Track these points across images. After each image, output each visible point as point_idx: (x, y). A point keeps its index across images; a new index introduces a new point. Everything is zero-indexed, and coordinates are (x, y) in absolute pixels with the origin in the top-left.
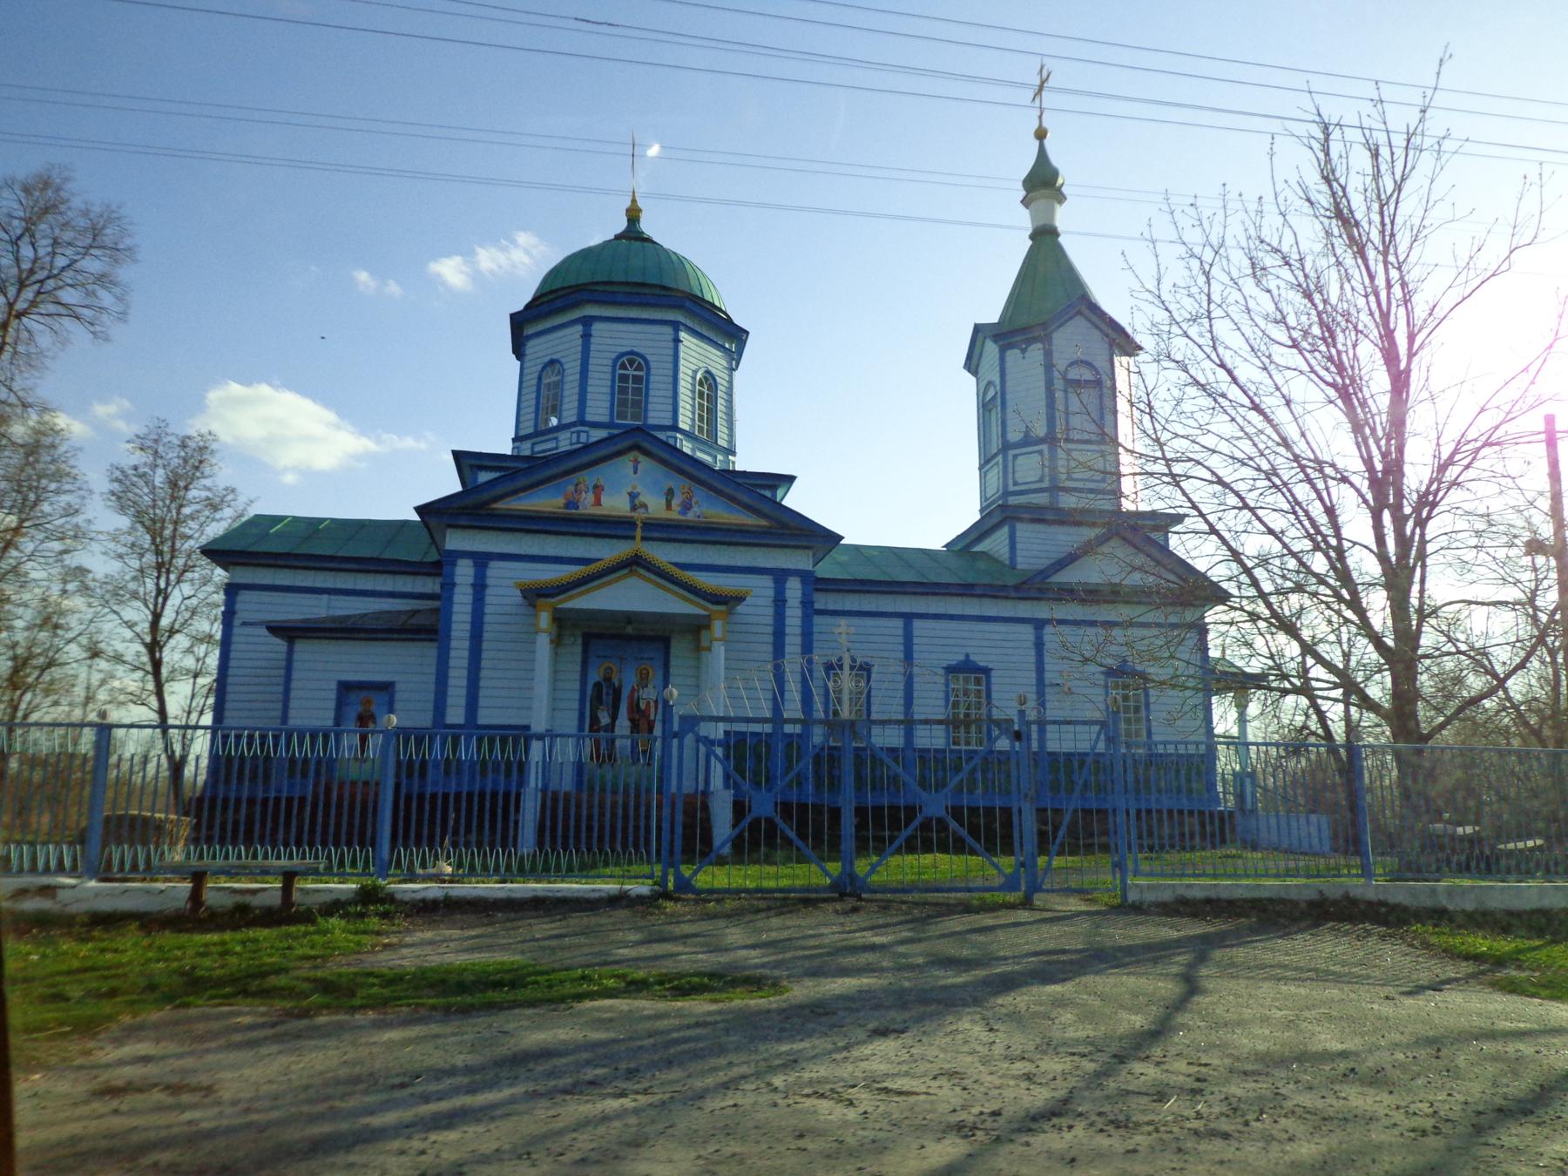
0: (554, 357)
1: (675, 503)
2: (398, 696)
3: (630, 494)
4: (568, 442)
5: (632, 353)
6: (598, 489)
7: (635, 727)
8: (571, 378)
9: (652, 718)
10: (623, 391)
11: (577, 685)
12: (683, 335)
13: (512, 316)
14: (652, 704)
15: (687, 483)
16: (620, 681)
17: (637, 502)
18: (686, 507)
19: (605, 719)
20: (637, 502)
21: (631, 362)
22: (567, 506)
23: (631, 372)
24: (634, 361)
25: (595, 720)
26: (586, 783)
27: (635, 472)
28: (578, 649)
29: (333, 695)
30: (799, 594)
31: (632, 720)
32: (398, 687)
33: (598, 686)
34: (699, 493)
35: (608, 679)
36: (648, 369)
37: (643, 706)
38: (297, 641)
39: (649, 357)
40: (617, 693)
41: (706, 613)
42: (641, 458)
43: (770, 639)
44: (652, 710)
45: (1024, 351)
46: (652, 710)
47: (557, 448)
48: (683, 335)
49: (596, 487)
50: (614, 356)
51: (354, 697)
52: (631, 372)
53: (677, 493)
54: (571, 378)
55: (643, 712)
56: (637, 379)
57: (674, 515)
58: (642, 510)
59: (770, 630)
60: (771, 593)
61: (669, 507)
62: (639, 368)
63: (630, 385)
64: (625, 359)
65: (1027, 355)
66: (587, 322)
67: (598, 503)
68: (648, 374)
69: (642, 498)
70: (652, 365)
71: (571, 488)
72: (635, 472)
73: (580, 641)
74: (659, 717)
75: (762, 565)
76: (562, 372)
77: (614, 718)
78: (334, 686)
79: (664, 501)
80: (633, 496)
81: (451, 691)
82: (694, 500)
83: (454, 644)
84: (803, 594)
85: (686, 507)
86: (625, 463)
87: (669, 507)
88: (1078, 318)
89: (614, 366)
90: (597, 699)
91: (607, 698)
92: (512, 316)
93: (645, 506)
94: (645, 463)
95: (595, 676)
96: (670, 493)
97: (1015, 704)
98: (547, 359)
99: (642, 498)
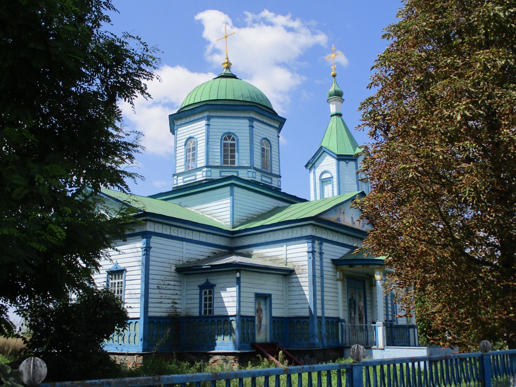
0: (192, 135)
2: (273, 301)
4: (201, 176)
8: (202, 148)
10: (225, 151)
13: (170, 116)
23: (229, 142)
26: (240, 268)
32: (273, 297)
36: (238, 140)
45: (347, 163)
47: (184, 178)
52: (229, 142)
54: (202, 148)
65: (348, 165)
76: (196, 143)
78: (253, 295)
88: (325, 153)
92: (170, 116)
98: (188, 136)
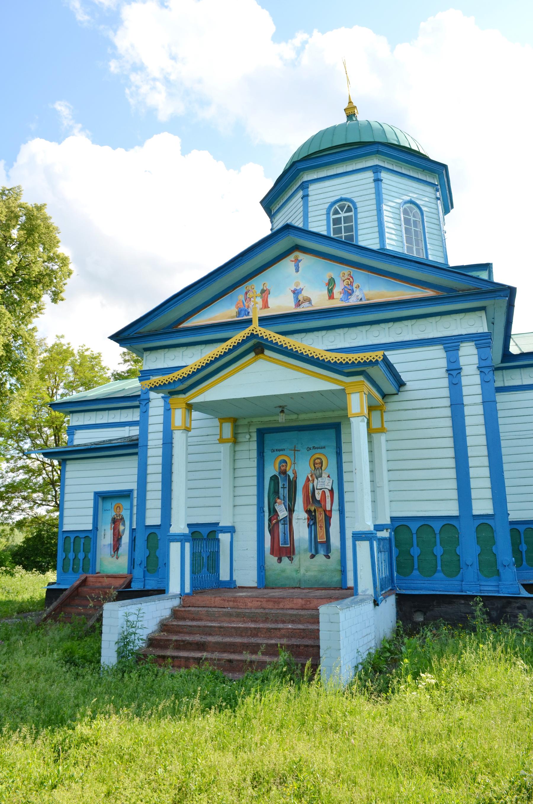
1: (337, 291)
3: (294, 292)
5: (341, 200)
6: (265, 293)
7: (312, 516)
9: (328, 508)
11: (254, 481)
12: (384, 175)
13: (261, 202)
14: (328, 494)
15: (346, 270)
16: (295, 473)
17: (300, 297)
18: (348, 292)
19: (283, 513)
20: (300, 297)
21: (342, 208)
22: (239, 314)
23: (342, 215)
24: (351, 211)
25: (273, 512)
27: (297, 270)
28: (254, 446)
29: (91, 504)
30: (475, 360)
31: (308, 512)
33: (274, 479)
34: (360, 277)
35: (284, 472)
37: (318, 497)
38: (68, 462)
39: (355, 200)
40: (292, 485)
41: (343, 388)
42: (301, 256)
43: (448, 412)
44: (328, 500)
46: (328, 500)
48: (384, 175)
49: (263, 291)
50: (327, 206)
51: (111, 505)
52: (342, 215)
53: (338, 281)
55: (319, 502)
56: (347, 220)
57: (337, 303)
58: (306, 304)
59: (447, 402)
60: (444, 363)
61: (331, 297)
62: (349, 210)
63: (343, 225)
64: (336, 206)
66: (304, 186)
67: (266, 305)
68: (356, 214)
69: (305, 294)
70: (358, 205)
71: (242, 297)
72: (297, 270)
73: (254, 437)
74: (336, 506)
75: (431, 336)
77: (291, 510)
78: (92, 496)
79: (326, 292)
80: (296, 293)
81: (149, 495)
82: (355, 285)
83: (150, 452)
84: (480, 359)
85: (348, 292)
86: (288, 264)
87: (331, 297)
89: (328, 214)
90: (275, 492)
91: (283, 492)
93: (309, 300)
94: (306, 260)
95: (271, 471)
96: (331, 283)
97: (194, 424)
99: (305, 294)
